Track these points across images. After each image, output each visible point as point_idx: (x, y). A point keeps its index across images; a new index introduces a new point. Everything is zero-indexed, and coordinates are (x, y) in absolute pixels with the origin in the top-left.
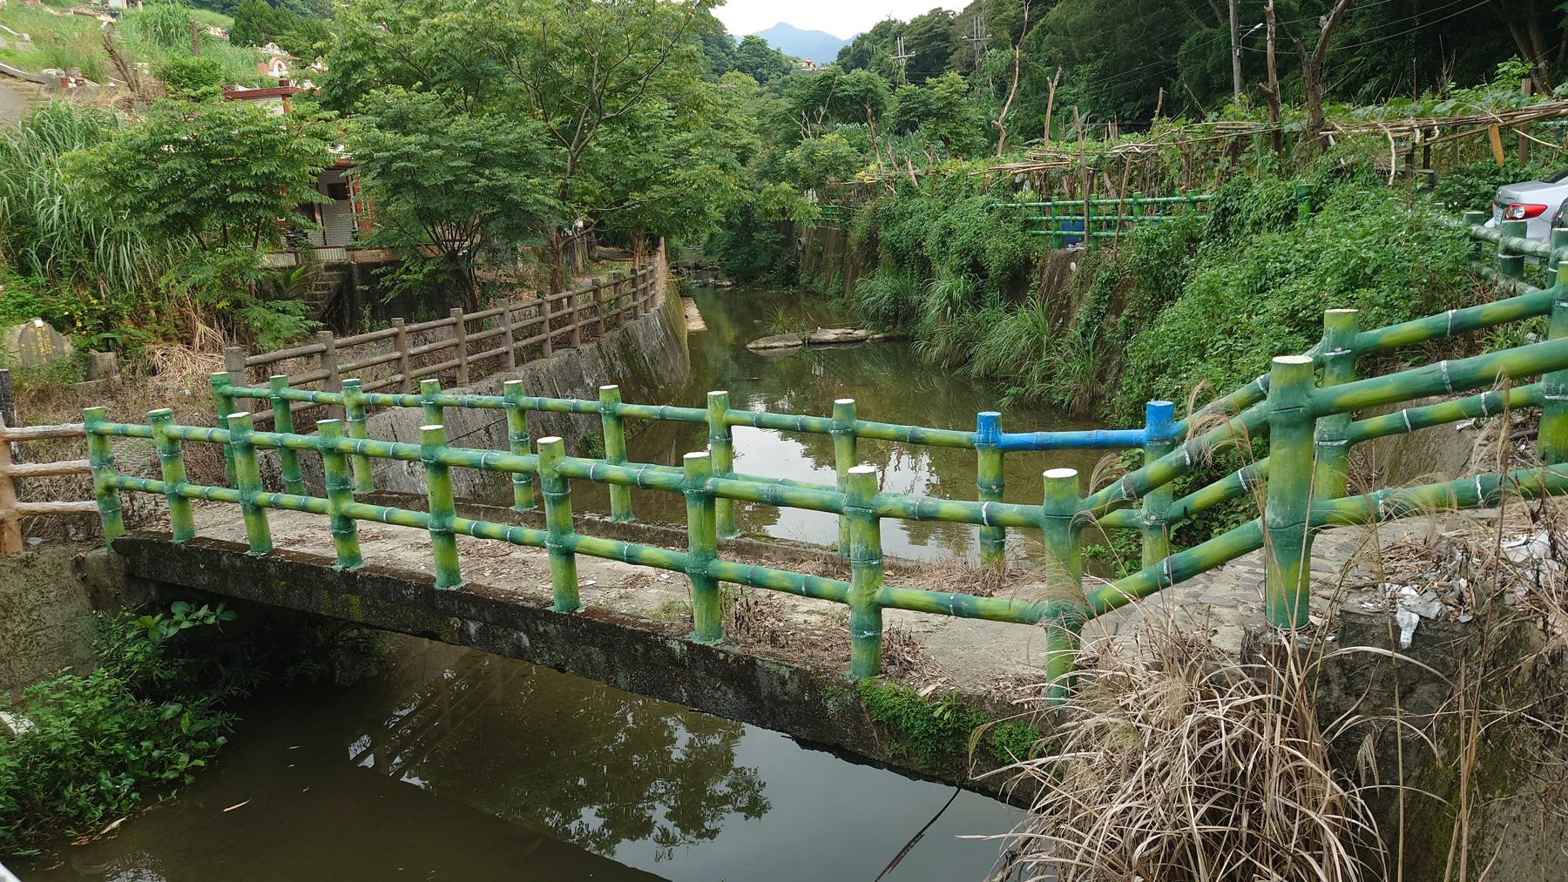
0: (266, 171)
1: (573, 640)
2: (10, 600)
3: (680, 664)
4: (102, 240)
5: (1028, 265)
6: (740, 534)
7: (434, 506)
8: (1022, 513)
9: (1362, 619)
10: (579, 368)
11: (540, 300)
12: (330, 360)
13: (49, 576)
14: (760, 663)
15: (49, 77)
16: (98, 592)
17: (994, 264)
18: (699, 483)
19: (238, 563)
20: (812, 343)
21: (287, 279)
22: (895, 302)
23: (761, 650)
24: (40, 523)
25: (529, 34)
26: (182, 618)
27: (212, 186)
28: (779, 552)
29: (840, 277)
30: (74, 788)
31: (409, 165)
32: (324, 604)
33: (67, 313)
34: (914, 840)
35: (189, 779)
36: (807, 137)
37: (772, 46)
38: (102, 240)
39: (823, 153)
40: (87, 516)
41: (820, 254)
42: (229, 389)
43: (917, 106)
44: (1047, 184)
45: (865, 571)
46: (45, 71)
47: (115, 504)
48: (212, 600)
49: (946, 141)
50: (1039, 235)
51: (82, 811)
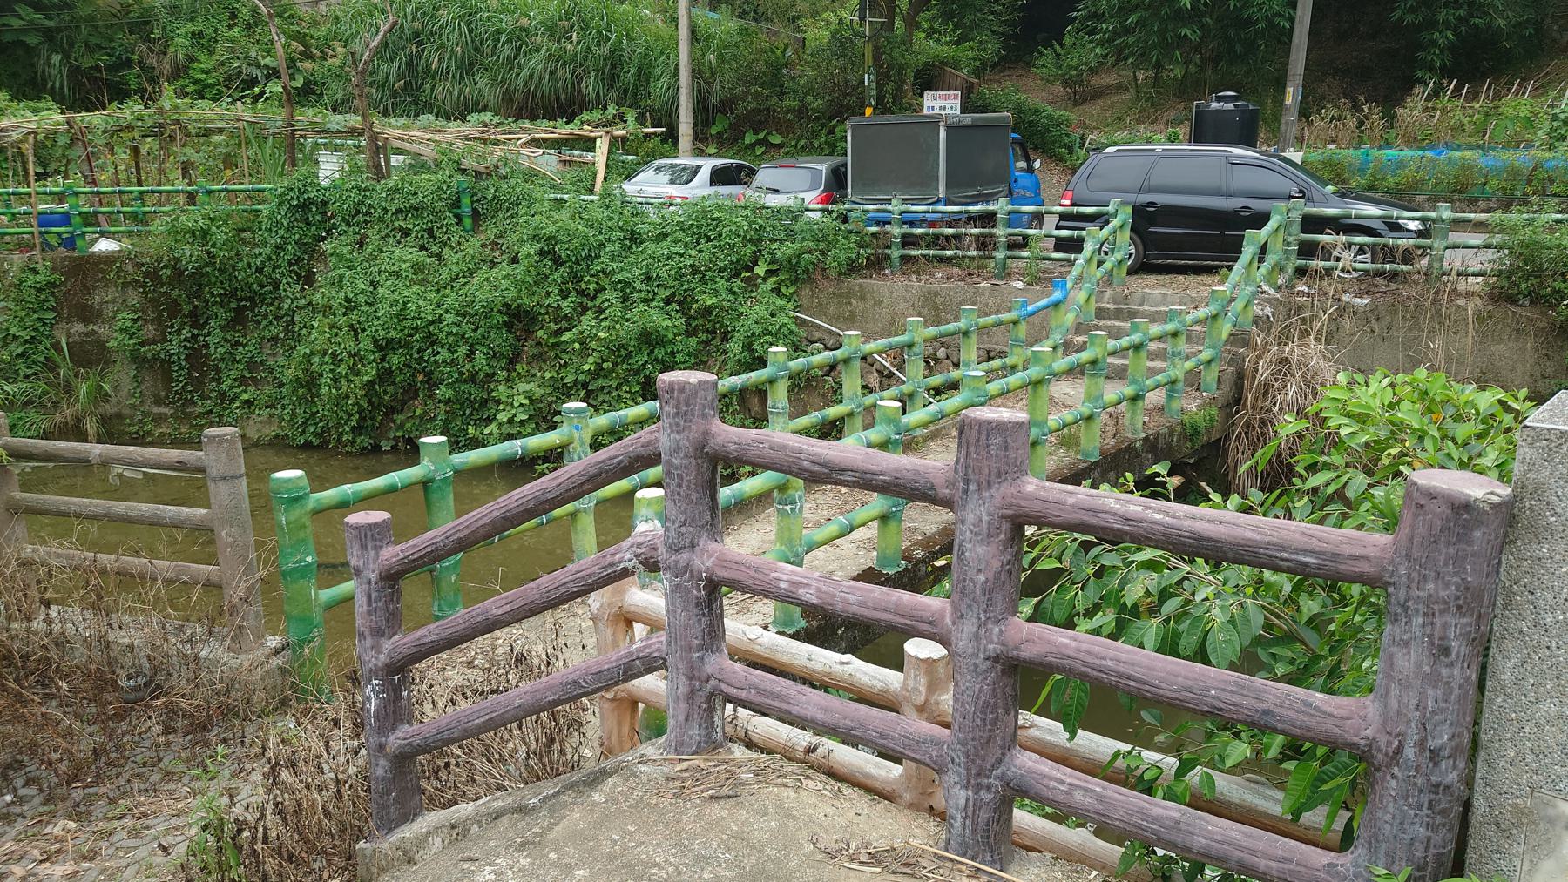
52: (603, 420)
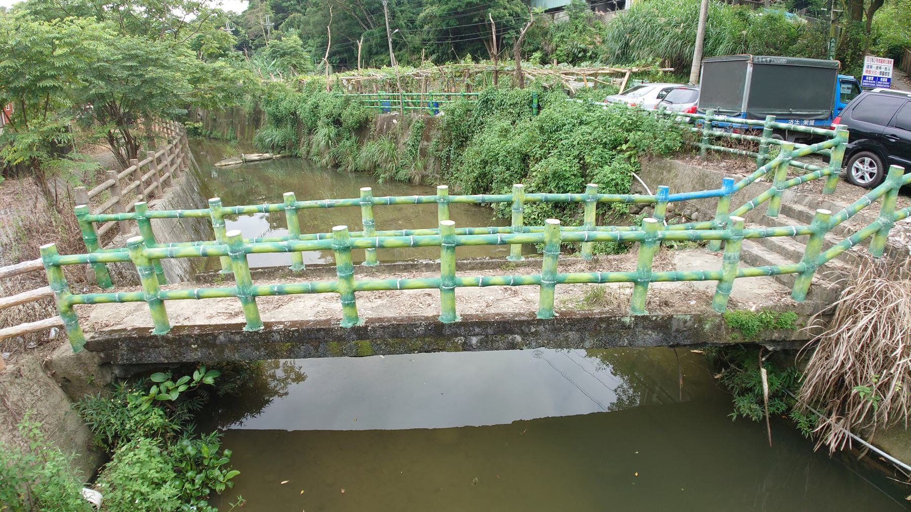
12: (118, 189)
13: (31, 380)
20: (246, 161)
52: (229, 209)
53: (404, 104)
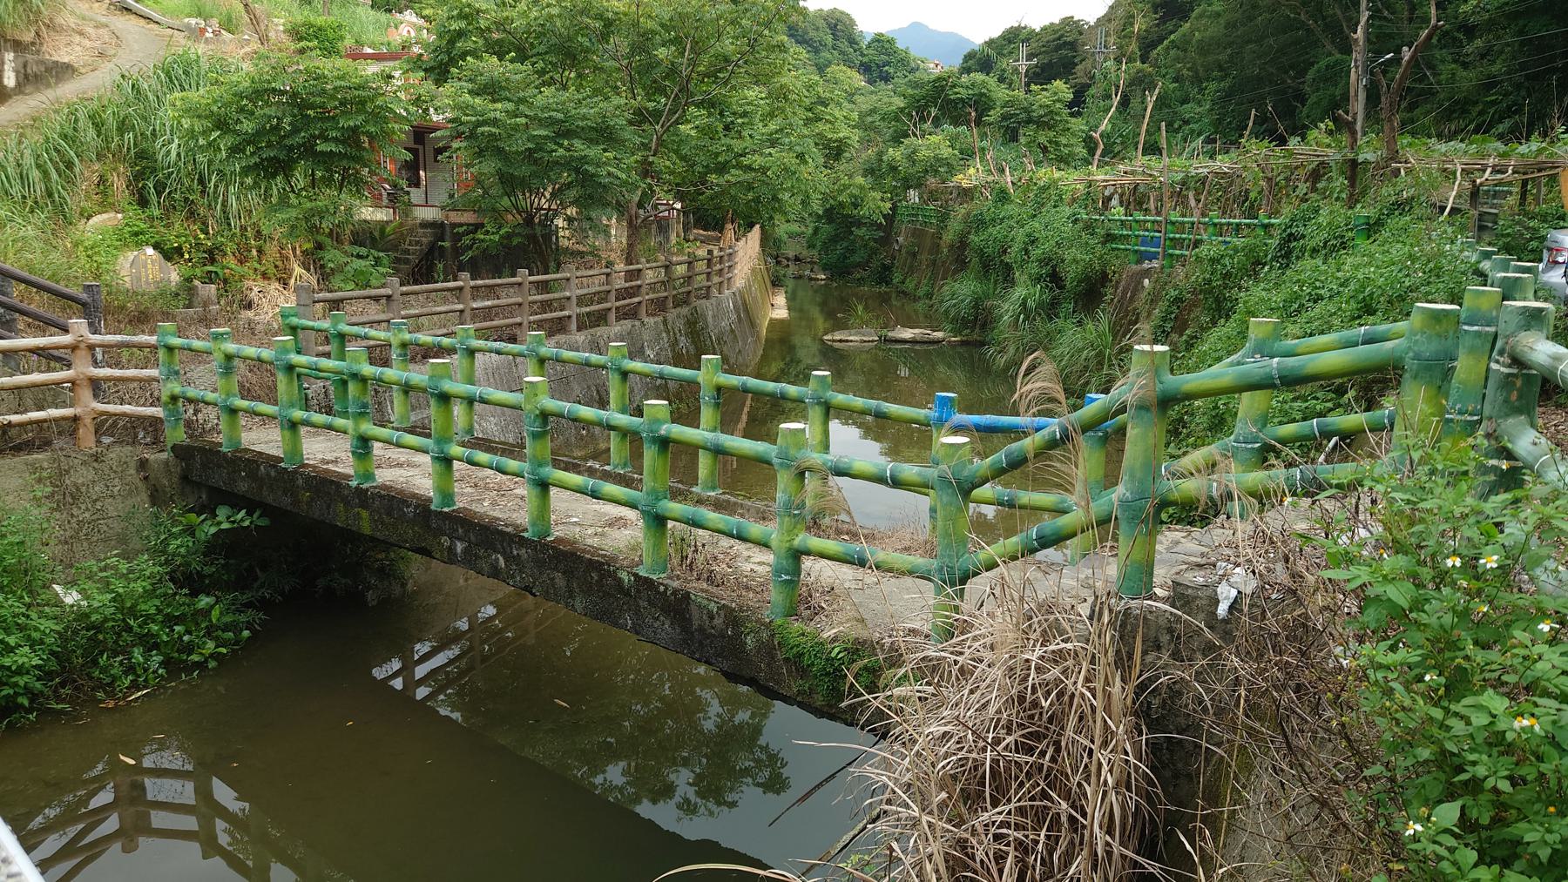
0: (352, 124)
1: (540, 564)
2: (78, 489)
3: (627, 593)
4: (213, 180)
5: (1104, 278)
6: (721, 491)
7: (436, 432)
8: (920, 474)
9: (1190, 591)
10: (642, 339)
11: (609, 270)
12: (394, 305)
13: (115, 472)
14: (693, 597)
15: (188, 26)
16: (157, 491)
17: (1071, 273)
18: (654, 427)
19: (273, 473)
21: (382, 231)
22: (976, 307)
23: (697, 588)
24: (115, 424)
25: (625, 15)
26: (224, 518)
27: (303, 134)
28: (752, 510)
29: (930, 278)
30: (108, 658)
31: (493, 130)
32: (340, 516)
33: (176, 245)
34: (827, 780)
35: (212, 664)
36: (915, 135)
37: (900, 45)
38: (213, 180)
39: (924, 153)
40: (155, 422)
41: (914, 255)
42: (295, 321)
43: (1018, 112)
44: (1135, 199)
45: (787, 519)
46: (186, 20)
47: (178, 412)
48: (251, 506)
49: (1045, 150)
50: (1119, 249)
51: (114, 679)
53: (1168, 243)
